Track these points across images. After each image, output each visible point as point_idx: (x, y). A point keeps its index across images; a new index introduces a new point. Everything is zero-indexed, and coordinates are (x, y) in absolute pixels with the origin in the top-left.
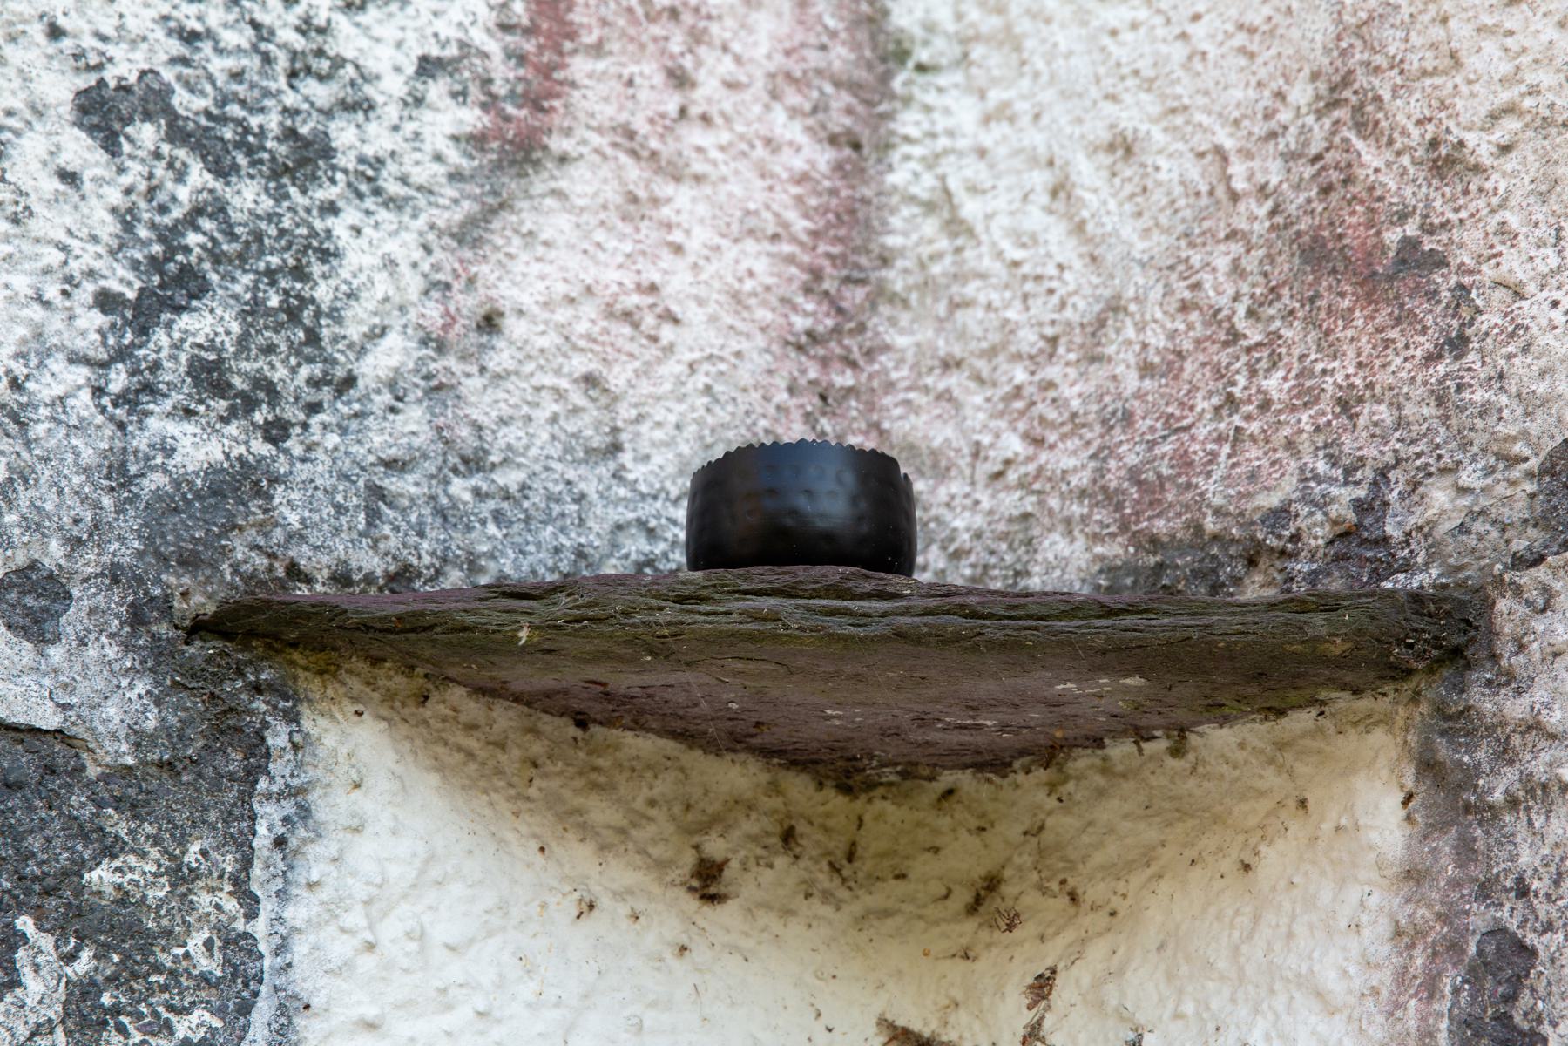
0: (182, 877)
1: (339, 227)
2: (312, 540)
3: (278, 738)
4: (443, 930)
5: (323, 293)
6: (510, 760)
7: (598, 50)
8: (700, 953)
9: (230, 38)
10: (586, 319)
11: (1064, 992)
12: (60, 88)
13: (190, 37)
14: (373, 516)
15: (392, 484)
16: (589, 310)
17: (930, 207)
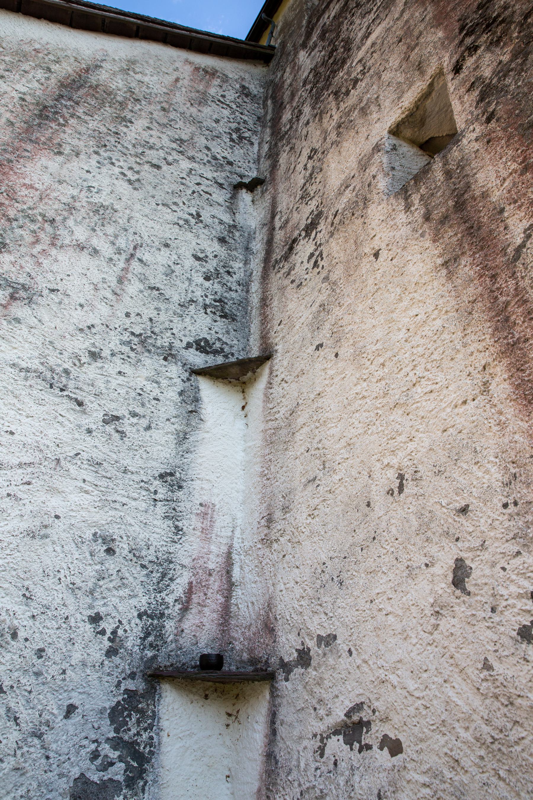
0: (148, 705)
1: (165, 623)
2: (466, 97)
3: (158, 688)
4: (176, 707)
5: (163, 632)
6: (184, 685)
7: (195, 594)
8: (205, 706)
9: (154, 603)
10: (194, 628)
11: (240, 712)
12: (136, 614)
13: (149, 604)
14: (169, 658)
15: (171, 653)
16: (194, 626)
17: (236, 605)
